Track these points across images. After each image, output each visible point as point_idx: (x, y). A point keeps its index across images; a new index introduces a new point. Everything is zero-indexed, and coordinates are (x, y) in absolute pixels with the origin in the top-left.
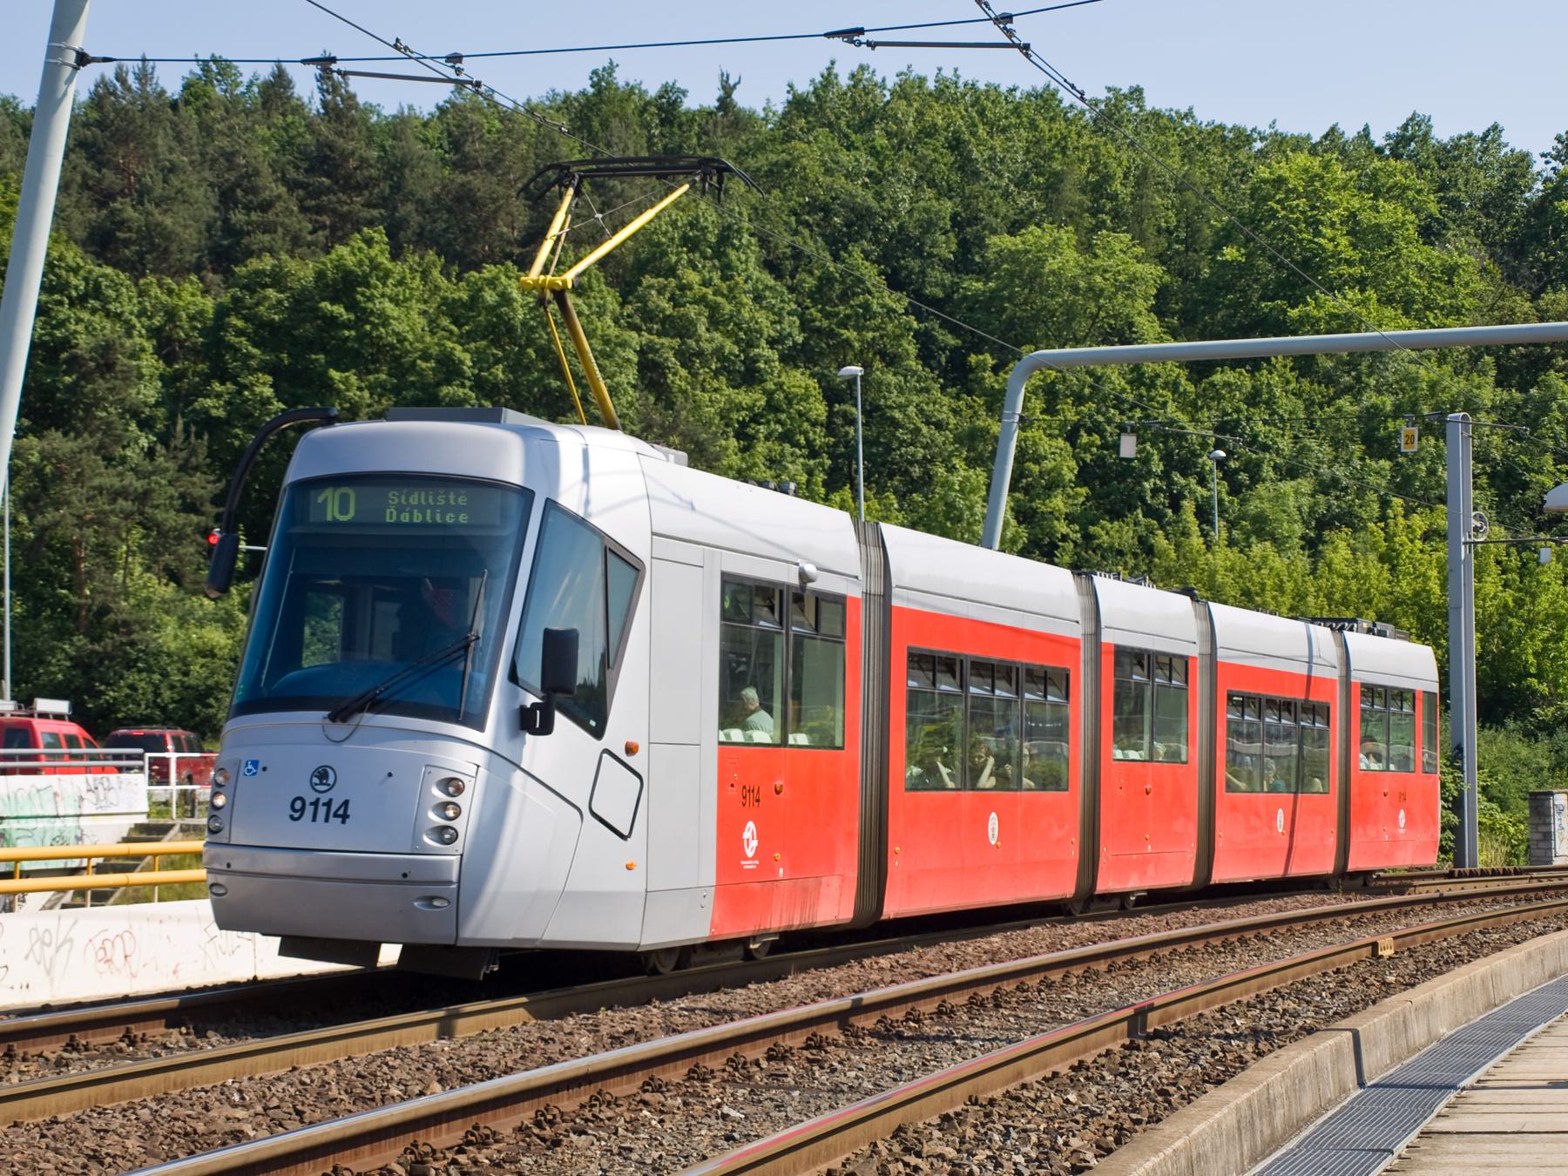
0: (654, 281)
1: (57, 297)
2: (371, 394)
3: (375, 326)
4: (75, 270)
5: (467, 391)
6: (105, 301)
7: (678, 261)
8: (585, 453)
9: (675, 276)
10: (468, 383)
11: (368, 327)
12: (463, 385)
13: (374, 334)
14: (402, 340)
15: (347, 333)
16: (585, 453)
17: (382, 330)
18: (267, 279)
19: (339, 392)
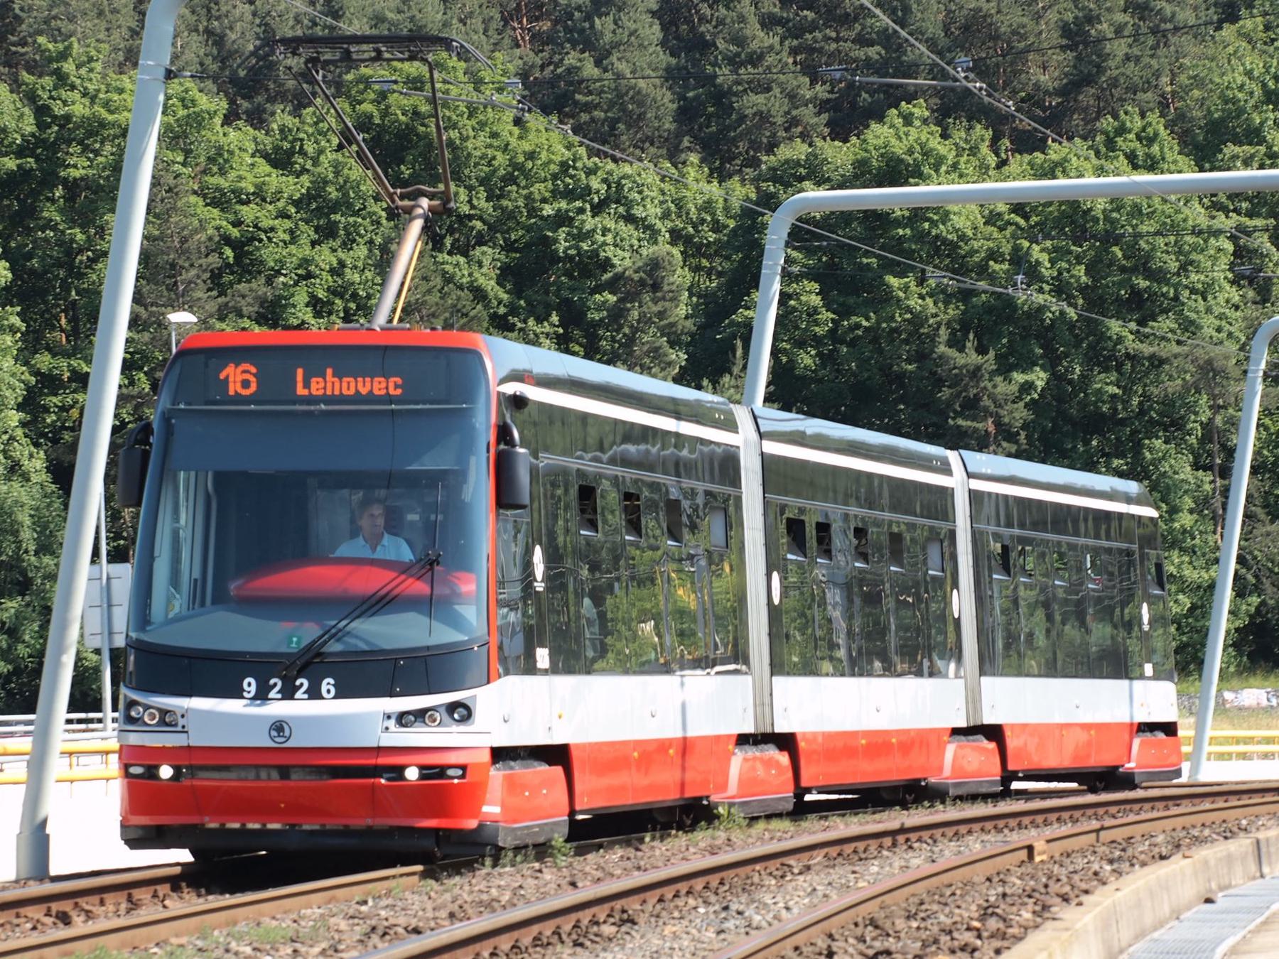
0: (1237, 149)
1: (578, 204)
2: (935, 303)
3: (934, 224)
4: (590, 172)
5: (1047, 296)
6: (629, 205)
7: (1262, 124)
8: (684, 706)
9: (1262, 141)
10: (1046, 287)
11: (926, 225)
12: (1041, 291)
13: (934, 232)
14: (963, 237)
15: (901, 232)
16: (684, 706)
17: (941, 227)
18: (802, 170)
19: (899, 300)
